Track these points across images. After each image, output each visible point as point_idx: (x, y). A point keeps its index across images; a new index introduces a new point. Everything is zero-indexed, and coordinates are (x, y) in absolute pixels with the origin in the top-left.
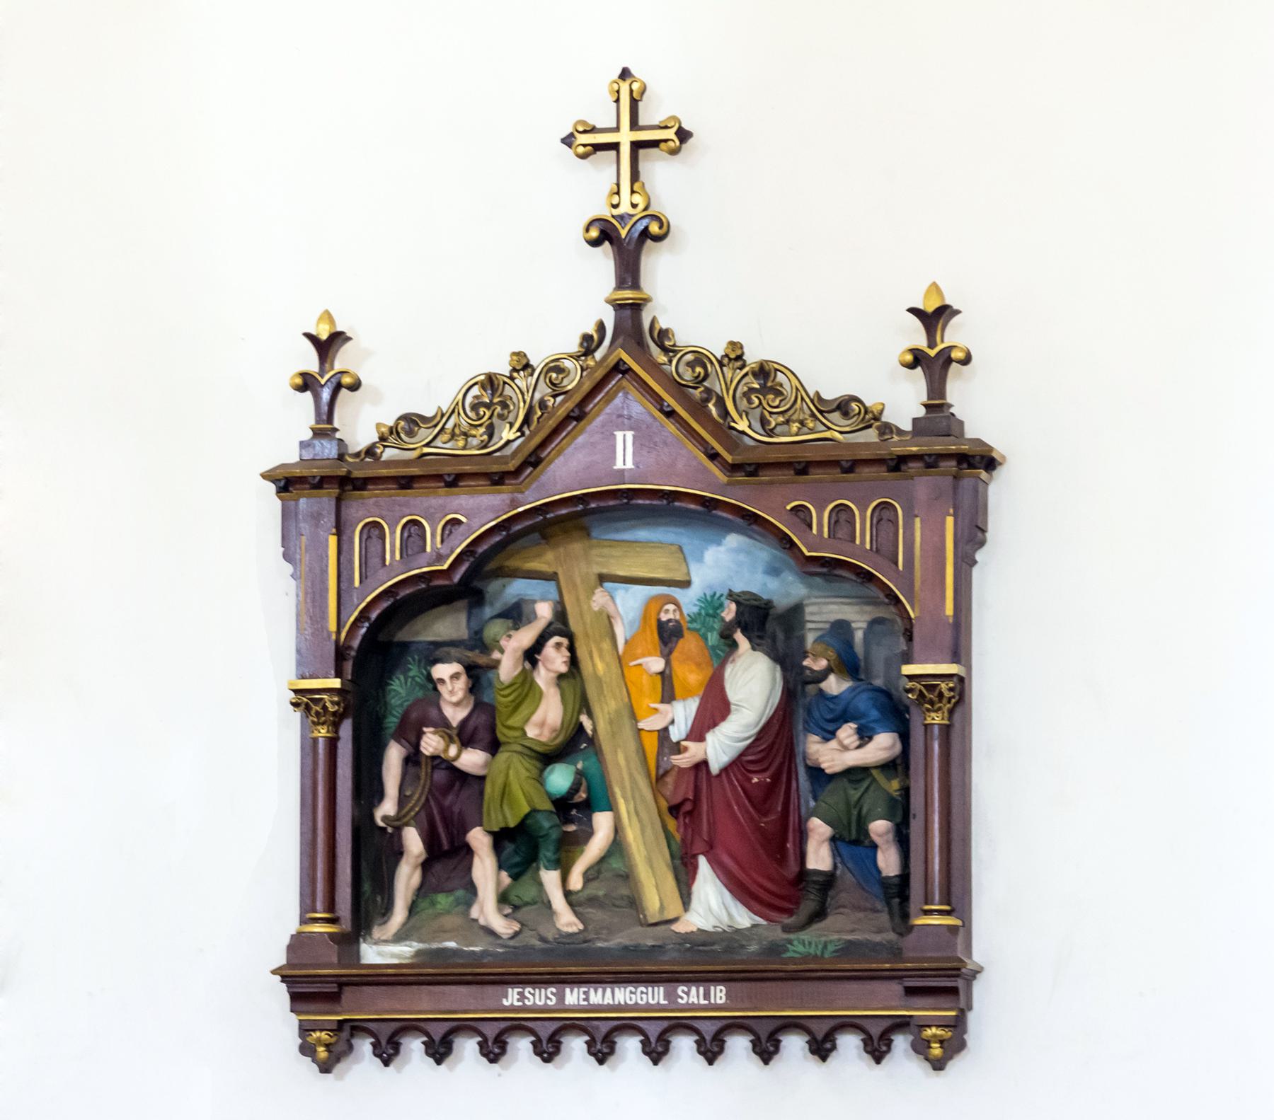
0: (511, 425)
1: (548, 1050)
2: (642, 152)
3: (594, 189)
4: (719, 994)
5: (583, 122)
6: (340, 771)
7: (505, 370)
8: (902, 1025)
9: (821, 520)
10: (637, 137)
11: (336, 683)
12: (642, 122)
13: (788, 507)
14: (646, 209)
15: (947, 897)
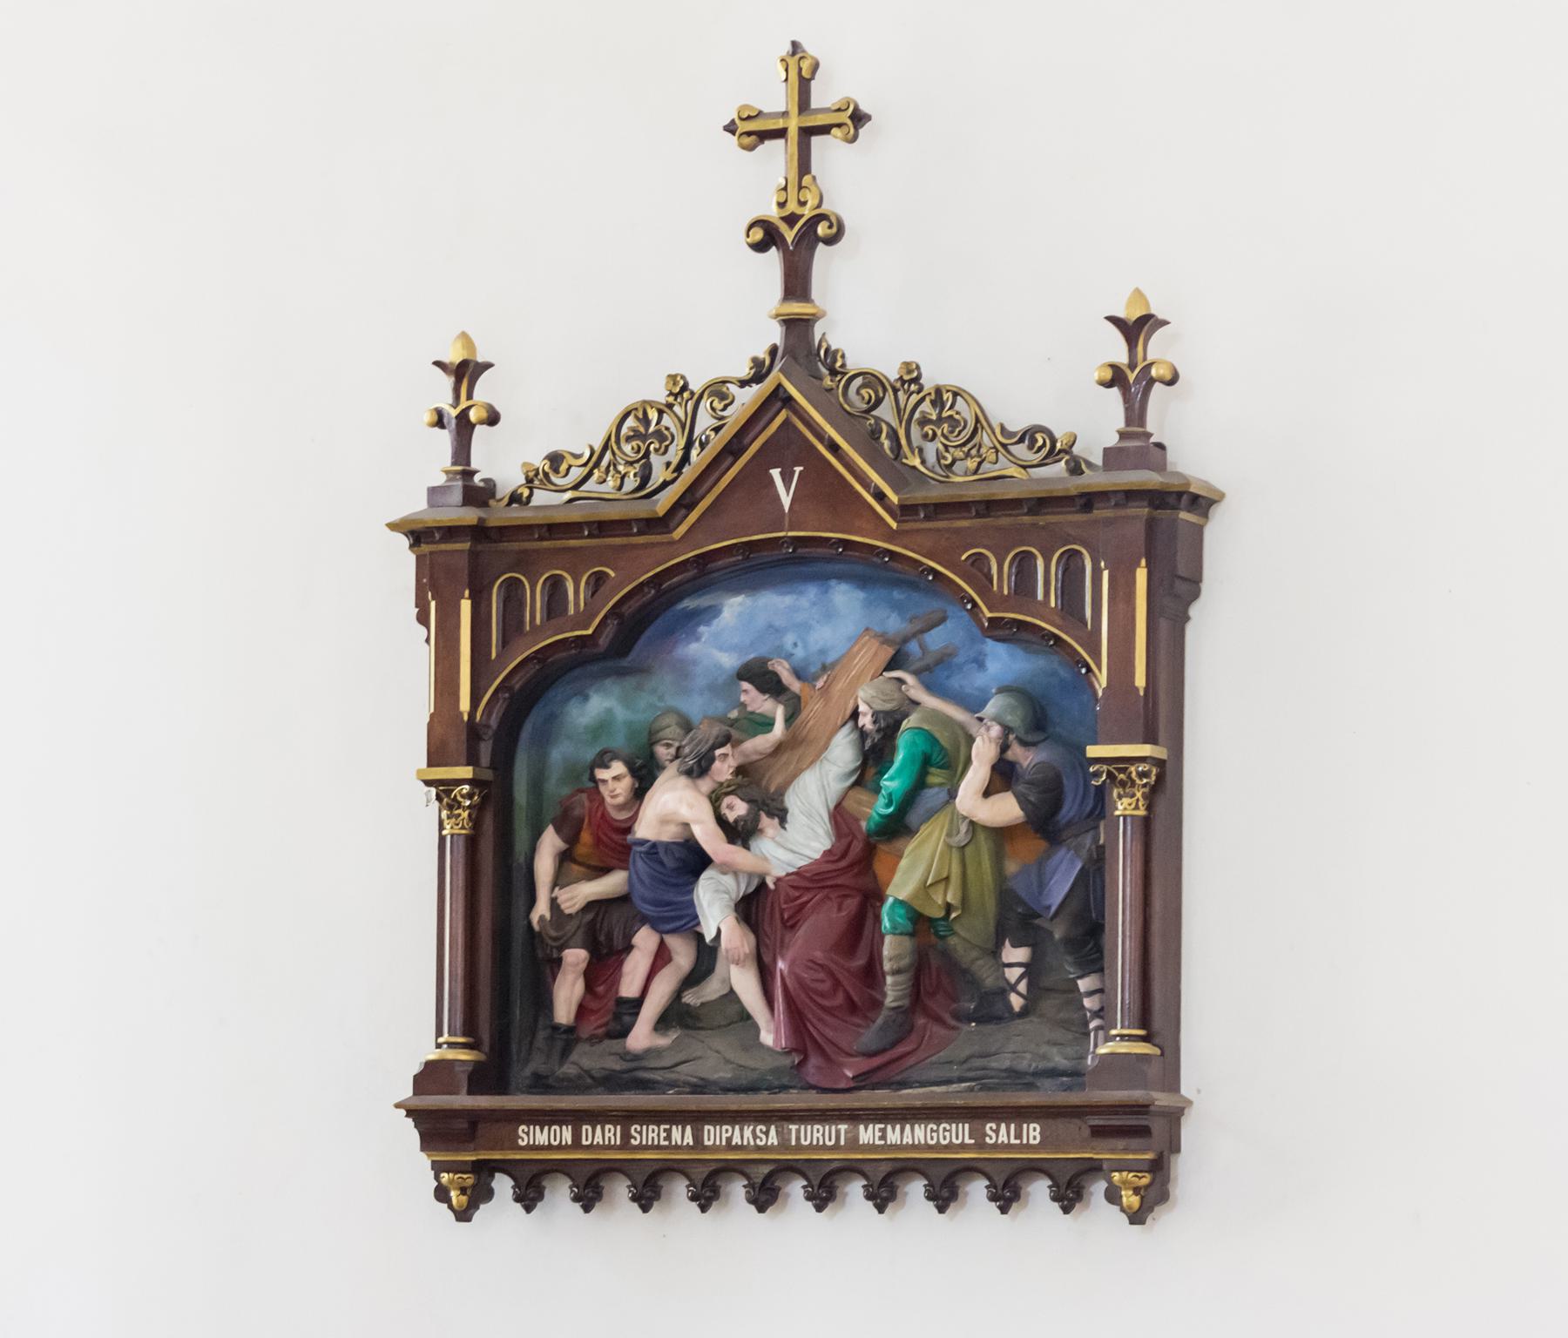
2: (816, 141)
3: (761, 180)
4: (1033, 1132)
8: (1094, 1169)
9: (1001, 573)
10: (804, 123)
12: (814, 105)
14: (819, 206)
15: (1144, 1017)
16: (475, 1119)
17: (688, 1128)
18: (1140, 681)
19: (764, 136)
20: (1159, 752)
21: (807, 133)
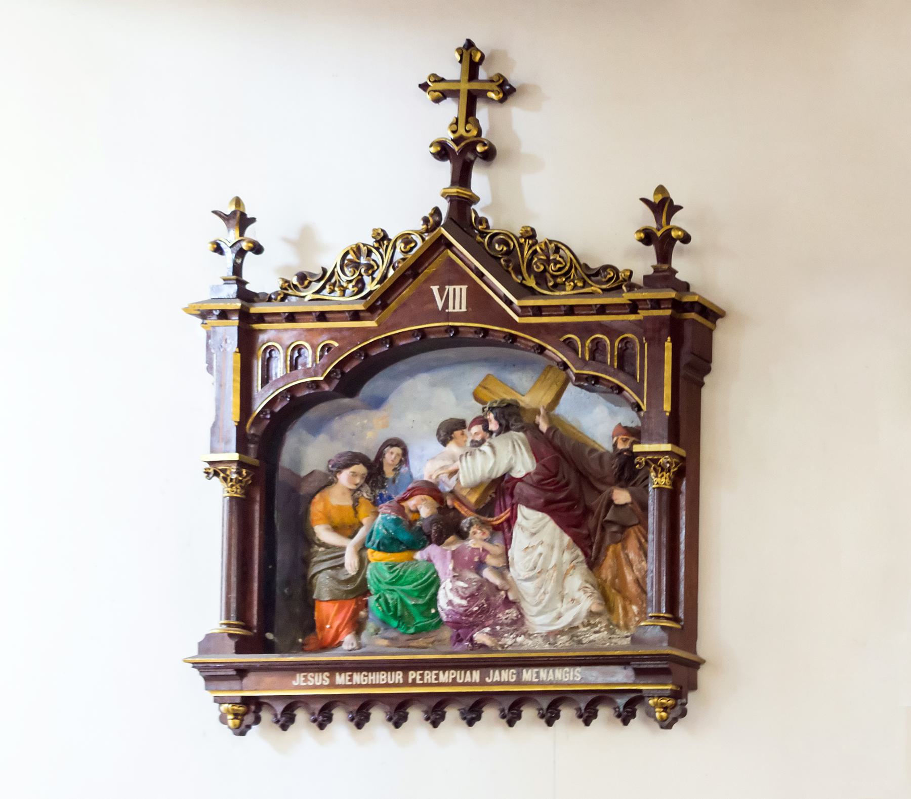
0: (373, 279)
1: (435, 717)
5: (434, 75)
11: (235, 457)
13: (562, 340)
16: (242, 672)
18: (667, 407)
20: (682, 452)
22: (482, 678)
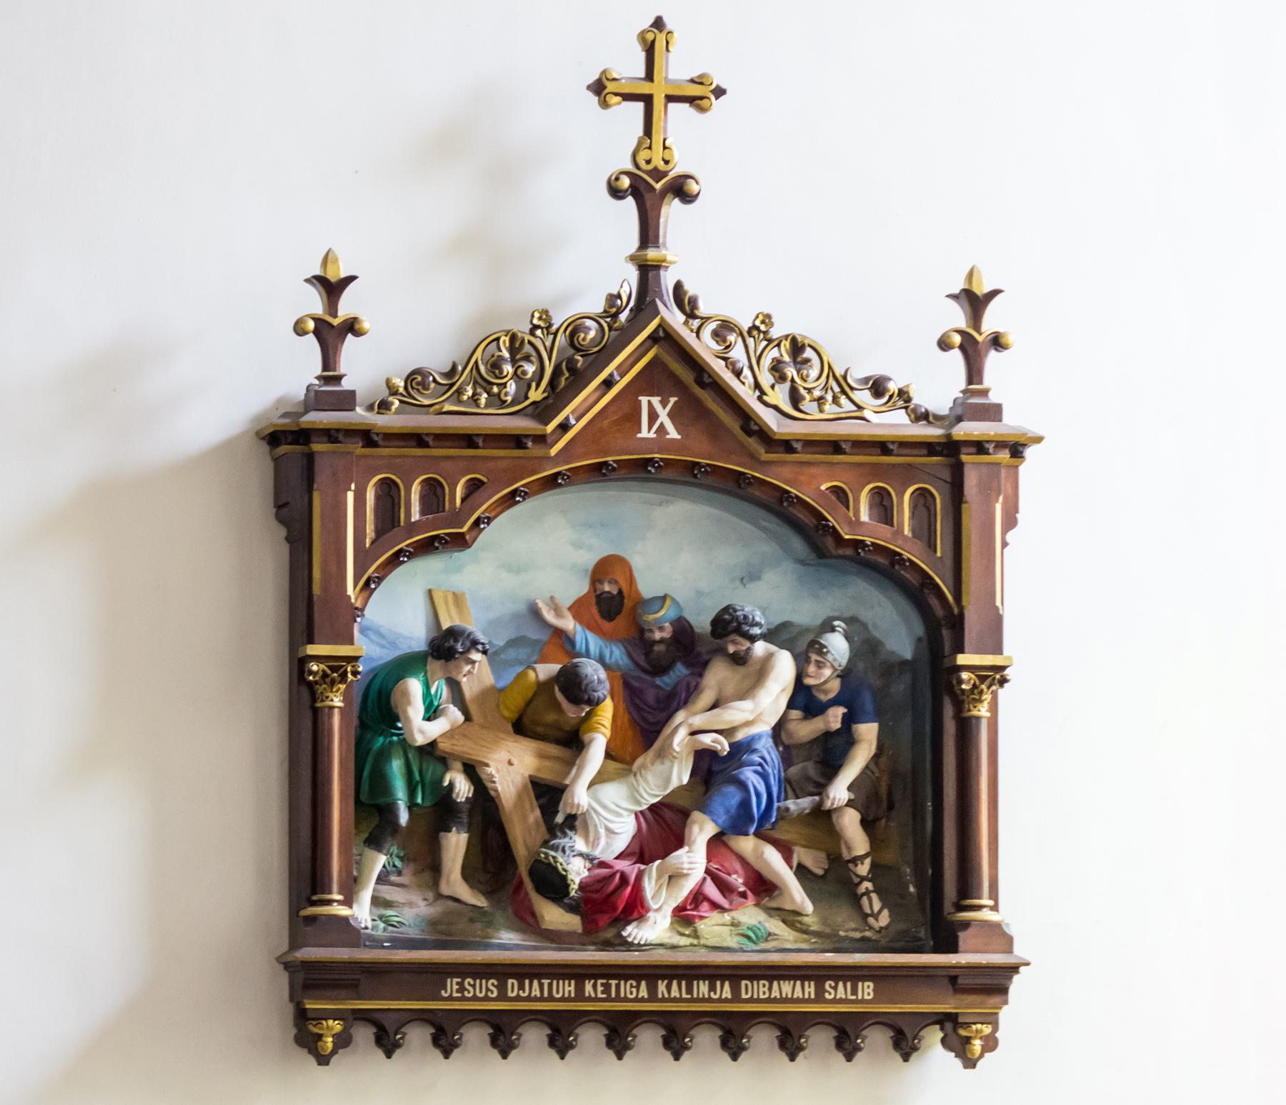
2: (640, 106)
4: (867, 990)
6: (977, 663)
7: (746, 325)
10: (649, 88)
12: (671, 105)
17: (727, 984)
19: (650, 50)
21: (647, 100)
22: (580, 995)
